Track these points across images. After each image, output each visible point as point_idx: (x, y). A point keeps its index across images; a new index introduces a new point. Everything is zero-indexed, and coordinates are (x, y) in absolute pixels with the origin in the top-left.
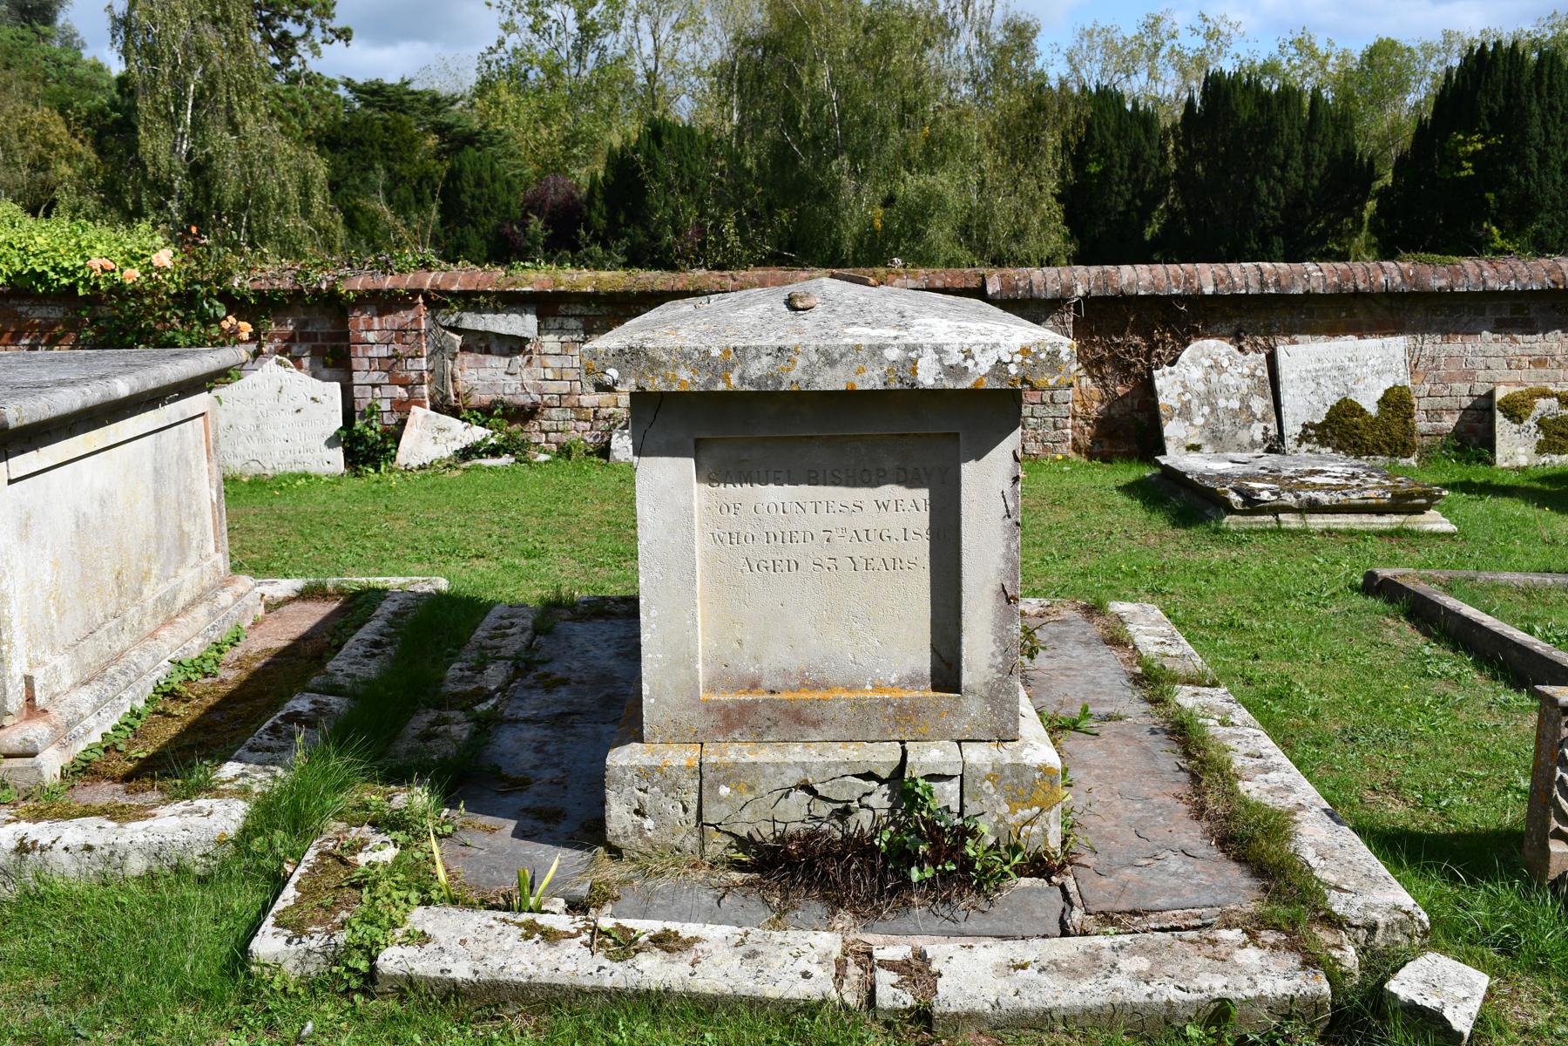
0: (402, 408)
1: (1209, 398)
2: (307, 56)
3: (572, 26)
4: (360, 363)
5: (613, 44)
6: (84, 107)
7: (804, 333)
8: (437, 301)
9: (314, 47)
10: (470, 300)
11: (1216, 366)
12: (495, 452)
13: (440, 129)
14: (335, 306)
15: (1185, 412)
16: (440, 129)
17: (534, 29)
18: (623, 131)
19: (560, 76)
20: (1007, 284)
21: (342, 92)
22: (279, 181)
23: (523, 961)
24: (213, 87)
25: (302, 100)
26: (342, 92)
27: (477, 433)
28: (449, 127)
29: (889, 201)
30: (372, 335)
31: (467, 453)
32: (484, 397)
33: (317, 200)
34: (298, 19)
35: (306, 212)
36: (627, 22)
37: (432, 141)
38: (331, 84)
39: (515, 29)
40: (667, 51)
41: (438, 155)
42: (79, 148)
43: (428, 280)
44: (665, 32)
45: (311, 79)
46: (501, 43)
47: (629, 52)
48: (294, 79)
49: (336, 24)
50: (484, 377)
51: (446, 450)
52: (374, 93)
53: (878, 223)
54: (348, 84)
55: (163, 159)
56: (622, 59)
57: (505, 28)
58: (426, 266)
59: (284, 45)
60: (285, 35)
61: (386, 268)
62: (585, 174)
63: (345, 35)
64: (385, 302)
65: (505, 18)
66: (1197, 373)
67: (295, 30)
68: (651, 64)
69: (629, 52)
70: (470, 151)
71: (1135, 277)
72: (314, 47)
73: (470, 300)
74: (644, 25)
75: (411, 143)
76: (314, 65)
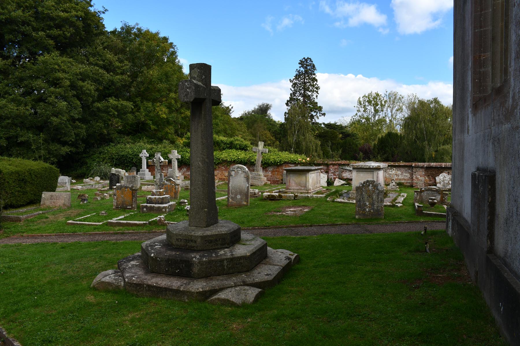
0: (335, 179)
1: (443, 181)
2: (316, 119)
3: (373, 110)
4: (330, 173)
5: (381, 115)
6: (273, 130)
7: (364, 164)
8: (340, 165)
9: (317, 117)
10: (344, 165)
11: (445, 177)
12: (346, 184)
13: (342, 133)
14: (327, 165)
15: (440, 183)
16: (342, 133)
17: (364, 111)
18: (385, 131)
19: (369, 121)
20: (415, 165)
21: (323, 126)
22: (312, 146)
23: (343, 201)
24: (301, 128)
25: (314, 128)
26: (323, 126)
27: (344, 182)
28: (344, 132)
29: (436, 151)
30: (332, 168)
31: (343, 185)
32: (345, 178)
33: (318, 149)
34: (315, 112)
35: (316, 151)
36: (385, 109)
37: (341, 136)
38: (321, 124)
39: (360, 111)
40: (394, 116)
41: (341, 139)
42: (272, 138)
43: (339, 162)
44: (394, 111)
45: (317, 123)
46: (357, 114)
47: (386, 116)
48: (313, 123)
49: (322, 112)
50: (346, 175)
51: (340, 184)
52: (329, 126)
53: (434, 156)
54: (324, 124)
55: (291, 141)
56: (384, 117)
57: (358, 111)
58: (339, 160)
59: (312, 117)
60: (312, 115)
61: (334, 161)
62: (373, 143)
63: (324, 114)
64: (334, 165)
65: (358, 109)
66: (442, 178)
67: (314, 114)
68: (390, 118)
69: (386, 116)
70: (349, 138)
71: (433, 164)
72: (317, 117)
73: (344, 165)
74: (389, 110)
75: (336, 137)
76: (317, 121)
